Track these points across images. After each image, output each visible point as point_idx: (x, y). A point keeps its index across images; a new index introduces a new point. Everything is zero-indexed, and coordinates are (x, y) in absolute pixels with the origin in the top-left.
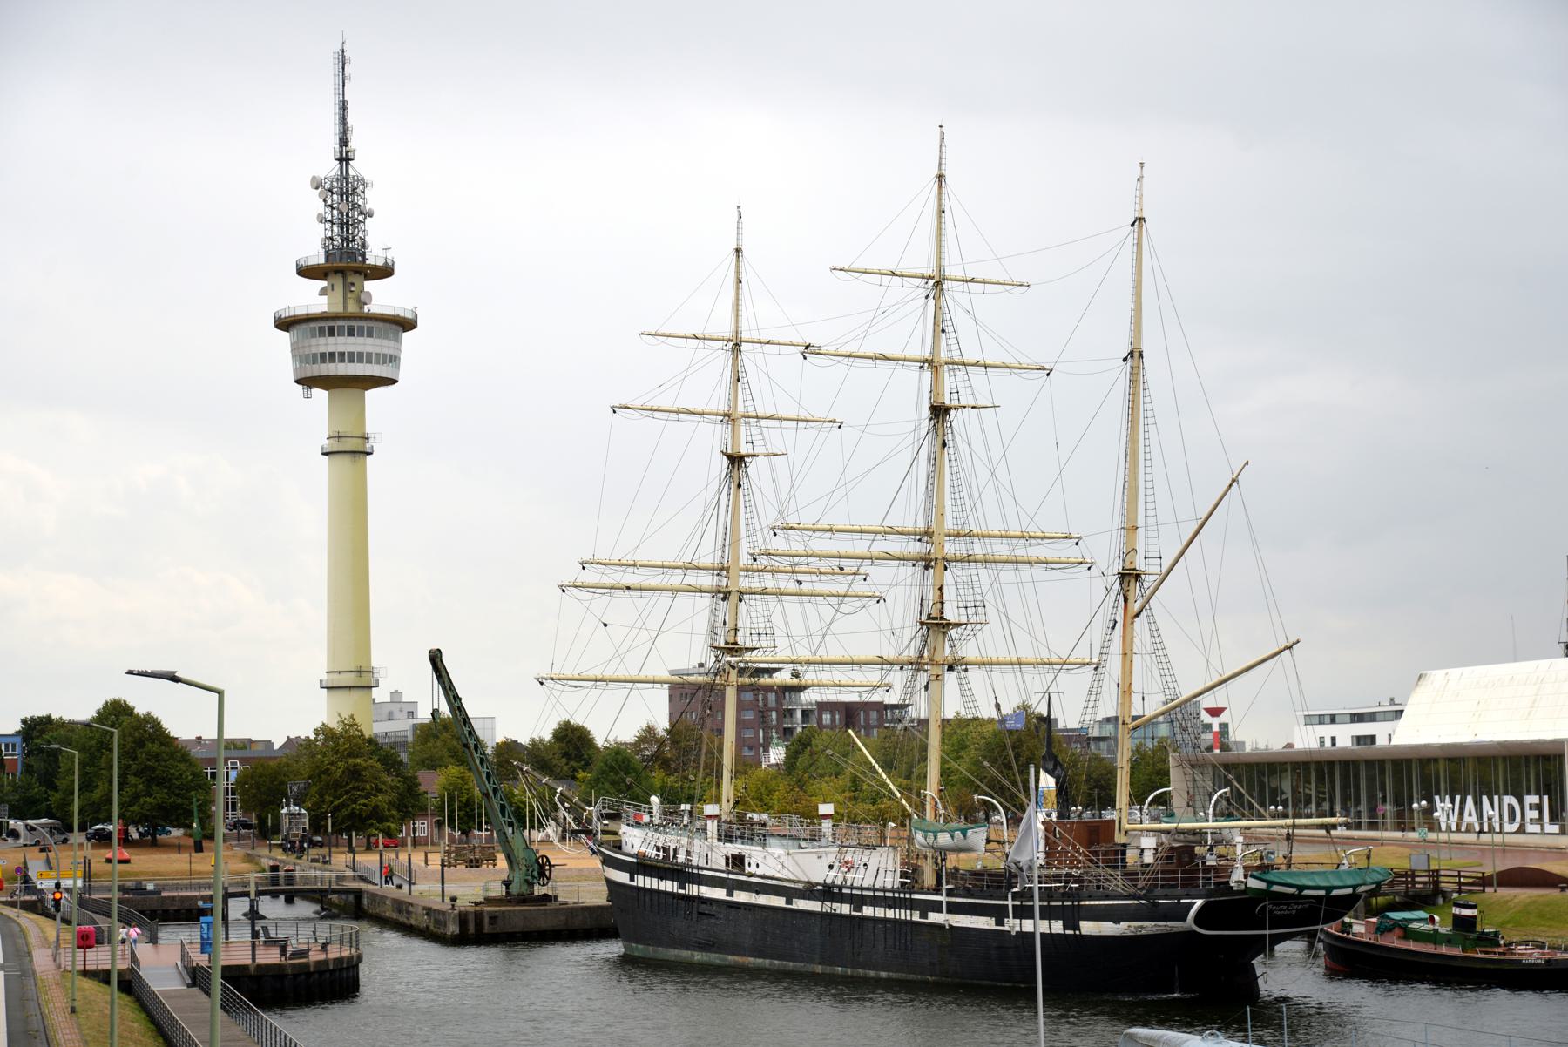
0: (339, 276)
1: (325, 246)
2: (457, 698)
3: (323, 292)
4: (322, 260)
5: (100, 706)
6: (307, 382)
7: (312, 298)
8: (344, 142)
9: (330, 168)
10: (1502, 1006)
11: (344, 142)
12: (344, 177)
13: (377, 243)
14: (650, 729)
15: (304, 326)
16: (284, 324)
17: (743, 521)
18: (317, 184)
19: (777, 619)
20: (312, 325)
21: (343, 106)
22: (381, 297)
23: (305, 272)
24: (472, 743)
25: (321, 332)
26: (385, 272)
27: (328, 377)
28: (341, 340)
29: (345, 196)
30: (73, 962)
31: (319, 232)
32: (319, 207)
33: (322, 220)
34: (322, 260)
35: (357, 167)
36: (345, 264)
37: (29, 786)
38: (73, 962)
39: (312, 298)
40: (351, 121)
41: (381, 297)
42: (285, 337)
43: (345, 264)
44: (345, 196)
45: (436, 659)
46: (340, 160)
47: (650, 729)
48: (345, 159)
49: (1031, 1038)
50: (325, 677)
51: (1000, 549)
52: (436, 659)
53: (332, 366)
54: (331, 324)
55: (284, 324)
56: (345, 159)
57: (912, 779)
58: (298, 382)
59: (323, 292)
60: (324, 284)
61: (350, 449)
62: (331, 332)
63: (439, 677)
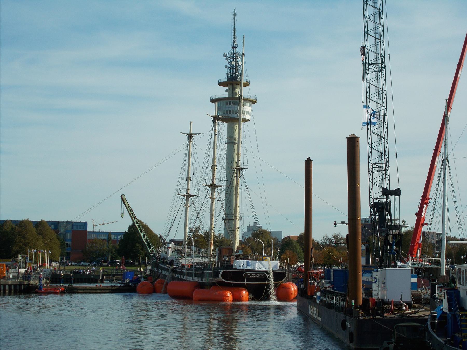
2: (131, 210)
3: (227, 91)
4: (226, 80)
5: (148, 224)
7: (223, 92)
8: (234, 42)
9: (229, 50)
14: (85, 224)
16: (213, 101)
23: (221, 84)
25: (227, 104)
26: (247, 84)
31: (227, 71)
32: (226, 63)
33: (226, 67)
34: (226, 80)
36: (232, 82)
39: (223, 92)
41: (245, 92)
45: (308, 163)
46: (233, 47)
47: (85, 224)
52: (308, 163)
55: (213, 101)
57: (278, 283)
59: (227, 91)
60: (227, 88)
62: (230, 104)
63: (125, 204)
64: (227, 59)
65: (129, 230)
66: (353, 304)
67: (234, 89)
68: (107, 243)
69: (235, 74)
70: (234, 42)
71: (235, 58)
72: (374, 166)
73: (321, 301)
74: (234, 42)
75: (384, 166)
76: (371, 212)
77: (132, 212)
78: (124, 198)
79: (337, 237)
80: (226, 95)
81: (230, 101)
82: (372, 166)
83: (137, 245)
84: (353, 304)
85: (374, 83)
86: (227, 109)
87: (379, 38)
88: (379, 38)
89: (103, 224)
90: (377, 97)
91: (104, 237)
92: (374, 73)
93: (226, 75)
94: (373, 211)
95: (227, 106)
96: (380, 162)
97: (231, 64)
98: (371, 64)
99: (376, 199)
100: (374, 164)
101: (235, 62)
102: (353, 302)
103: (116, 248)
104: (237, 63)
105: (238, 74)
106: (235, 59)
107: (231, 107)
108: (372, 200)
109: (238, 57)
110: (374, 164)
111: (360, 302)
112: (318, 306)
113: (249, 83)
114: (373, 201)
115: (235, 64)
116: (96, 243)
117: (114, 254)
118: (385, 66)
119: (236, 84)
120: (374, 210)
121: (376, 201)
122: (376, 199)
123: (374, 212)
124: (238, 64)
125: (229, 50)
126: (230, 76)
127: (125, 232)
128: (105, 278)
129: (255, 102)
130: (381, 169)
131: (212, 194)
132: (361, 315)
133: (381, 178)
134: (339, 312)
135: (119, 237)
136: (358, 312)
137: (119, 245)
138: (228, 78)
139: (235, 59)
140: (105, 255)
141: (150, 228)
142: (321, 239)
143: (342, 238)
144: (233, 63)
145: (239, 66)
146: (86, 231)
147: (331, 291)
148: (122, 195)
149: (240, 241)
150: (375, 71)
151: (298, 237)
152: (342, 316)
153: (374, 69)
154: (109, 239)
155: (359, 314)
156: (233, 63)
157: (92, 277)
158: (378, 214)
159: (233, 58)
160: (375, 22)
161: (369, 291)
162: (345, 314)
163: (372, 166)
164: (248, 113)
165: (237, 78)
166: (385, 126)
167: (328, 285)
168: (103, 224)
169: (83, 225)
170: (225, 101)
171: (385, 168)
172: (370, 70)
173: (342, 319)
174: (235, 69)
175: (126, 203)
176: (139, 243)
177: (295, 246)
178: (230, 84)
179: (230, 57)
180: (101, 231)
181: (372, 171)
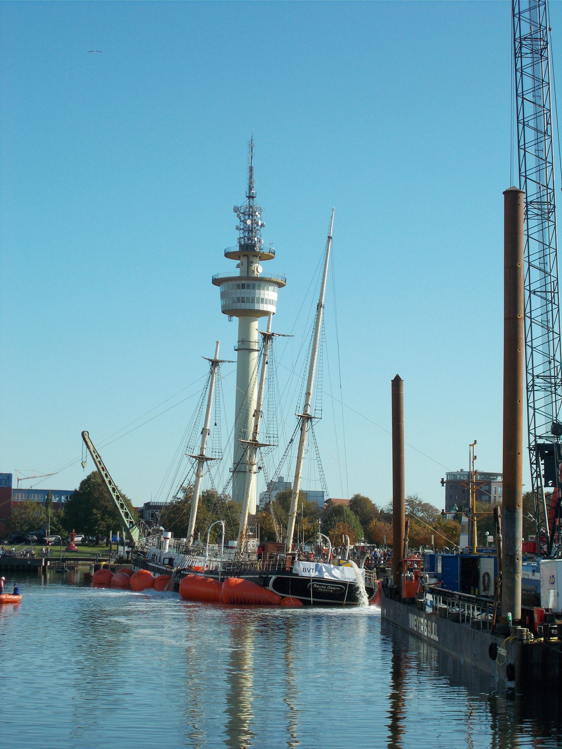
0: (246, 258)
1: (240, 243)
2: (98, 456)
3: (238, 266)
4: (237, 249)
7: (231, 268)
9: (243, 202)
13: (264, 241)
15: (225, 284)
16: (216, 282)
17: (321, 320)
18: (236, 210)
19: (210, 454)
20: (230, 283)
22: (260, 269)
23: (228, 255)
24: (107, 480)
25: (238, 287)
26: (269, 257)
27: (237, 310)
31: (238, 234)
32: (237, 222)
33: (238, 228)
34: (237, 249)
35: (257, 202)
36: (247, 252)
37: (453, 534)
39: (231, 268)
42: (217, 290)
43: (247, 252)
47: (9, 477)
49: (532, 537)
51: (544, 414)
53: (238, 304)
55: (216, 282)
58: (223, 312)
59: (238, 266)
60: (238, 262)
62: (243, 286)
63: (88, 447)
64: (238, 216)
65: (81, 488)
66: (511, 619)
67: (250, 264)
68: (45, 508)
69: (252, 240)
70: (250, 189)
71: (251, 215)
72: (537, 380)
73: (435, 608)
74: (250, 189)
75: (553, 381)
76: (531, 460)
77: (99, 459)
78: (86, 437)
79: (412, 501)
80: (236, 273)
81: (243, 282)
82: (533, 380)
83: (95, 511)
84: (511, 619)
85: (535, 236)
86: (238, 296)
87: (544, 158)
88: (544, 158)
89: (34, 477)
90: (542, 260)
91: (38, 497)
92: (536, 218)
93: (237, 241)
94: (534, 458)
95: (238, 291)
96: (547, 374)
97: (246, 223)
98: (531, 202)
99: (540, 437)
100: (538, 376)
101: (252, 221)
102: (510, 615)
103: (58, 516)
104: (255, 222)
105: (256, 239)
106: (252, 216)
107: (244, 293)
108: (532, 438)
109: (257, 213)
110: (538, 376)
111: (519, 616)
112: (429, 617)
113: (274, 254)
114: (535, 440)
115: (252, 224)
116: (26, 508)
117: (55, 526)
118: (554, 207)
119: (254, 256)
120: (537, 457)
121: (540, 441)
122: (540, 437)
123: (537, 459)
124: (257, 224)
125: (243, 202)
126: (243, 243)
127: (76, 491)
128: (49, 564)
129: (284, 285)
130: (549, 385)
131: (302, 425)
132: (525, 637)
133: (549, 400)
134: (479, 628)
135: (63, 498)
136: (521, 631)
137: (64, 512)
138: (241, 246)
139: (252, 216)
140: (40, 528)
141: (362, 495)
142: (387, 504)
143: (420, 503)
144: (249, 222)
145: (258, 228)
146: (10, 488)
147: (440, 591)
148: (83, 433)
149: (257, 507)
150: (537, 215)
151: (351, 501)
152: (489, 638)
153: (536, 211)
154: (47, 503)
155: (522, 636)
156: (249, 222)
157: (29, 562)
158: (543, 462)
159: (249, 215)
160: (536, 130)
161: (533, 598)
162: (493, 633)
163: (533, 380)
164: (270, 302)
165: (254, 246)
166: (555, 311)
167: (434, 581)
168: (34, 477)
169: (6, 478)
170: (235, 283)
171: (555, 383)
172: (529, 213)
173: (490, 643)
174: (252, 231)
175: (89, 444)
176: (97, 509)
177: (348, 516)
178: (244, 256)
179: (243, 213)
180: (33, 488)
181: (533, 388)
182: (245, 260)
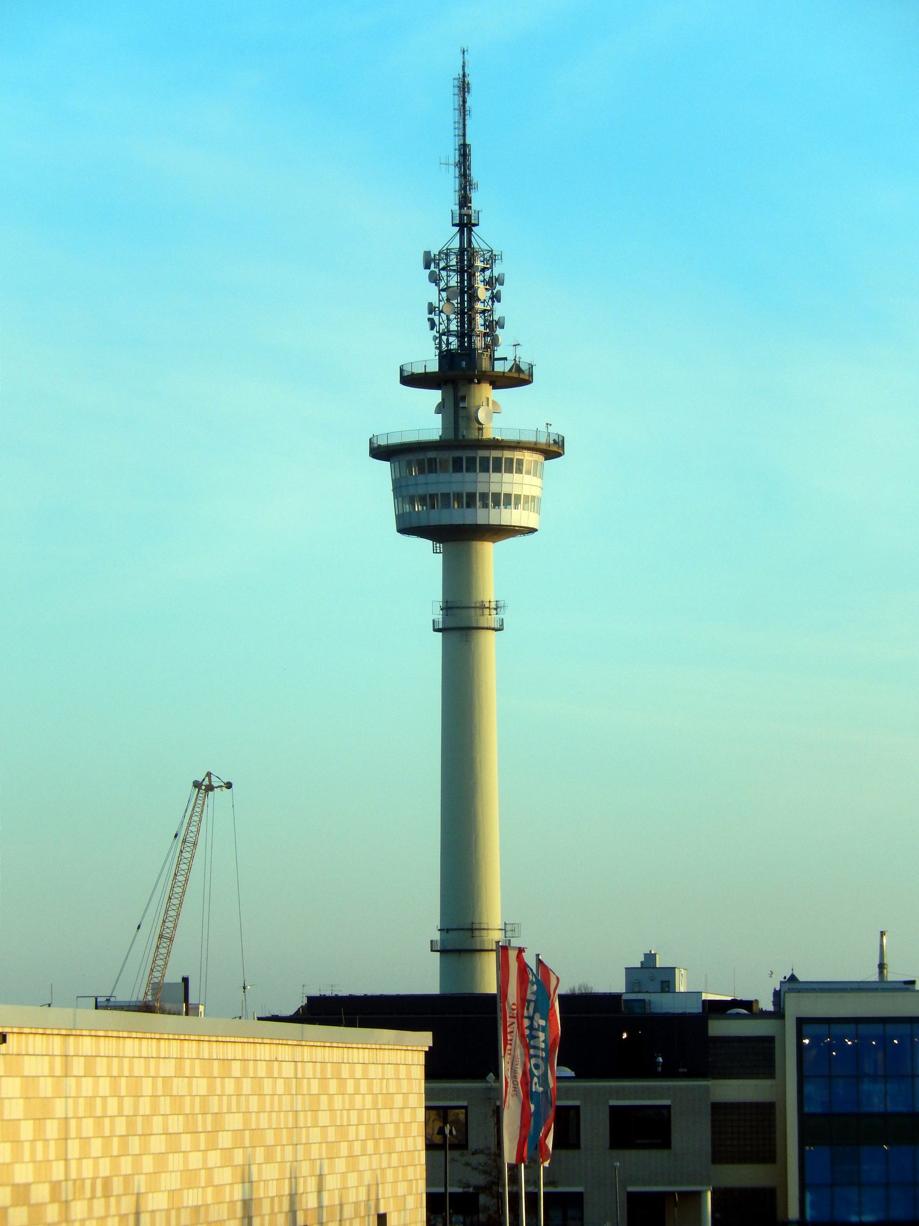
6: (407, 527)
7: (421, 417)
8: (464, 201)
9: (445, 237)
10: (467, 133)
11: (464, 201)
12: (466, 253)
21: (464, 152)
23: (411, 380)
26: (518, 378)
28: (444, 477)
29: (464, 274)
30: (348, 1054)
36: (460, 370)
38: (348, 1054)
39: (421, 417)
40: (476, 173)
41: (501, 414)
42: (385, 467)
44: (464, 274)
48: (465, 225)
50: (437, 936)
54: (457, 454)
55: (379, 452)
56: (465, 225)
61: (460, 622)
182: (450, 388)
